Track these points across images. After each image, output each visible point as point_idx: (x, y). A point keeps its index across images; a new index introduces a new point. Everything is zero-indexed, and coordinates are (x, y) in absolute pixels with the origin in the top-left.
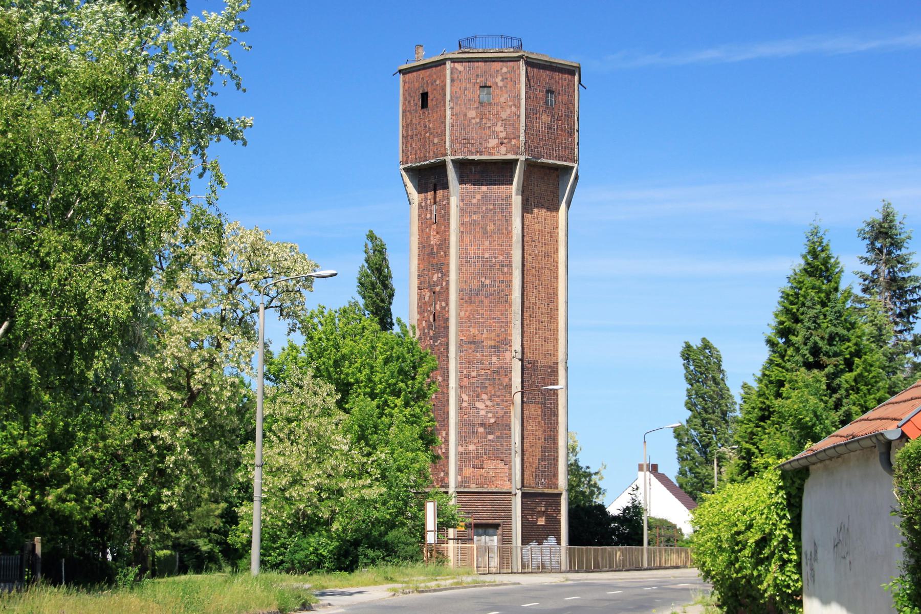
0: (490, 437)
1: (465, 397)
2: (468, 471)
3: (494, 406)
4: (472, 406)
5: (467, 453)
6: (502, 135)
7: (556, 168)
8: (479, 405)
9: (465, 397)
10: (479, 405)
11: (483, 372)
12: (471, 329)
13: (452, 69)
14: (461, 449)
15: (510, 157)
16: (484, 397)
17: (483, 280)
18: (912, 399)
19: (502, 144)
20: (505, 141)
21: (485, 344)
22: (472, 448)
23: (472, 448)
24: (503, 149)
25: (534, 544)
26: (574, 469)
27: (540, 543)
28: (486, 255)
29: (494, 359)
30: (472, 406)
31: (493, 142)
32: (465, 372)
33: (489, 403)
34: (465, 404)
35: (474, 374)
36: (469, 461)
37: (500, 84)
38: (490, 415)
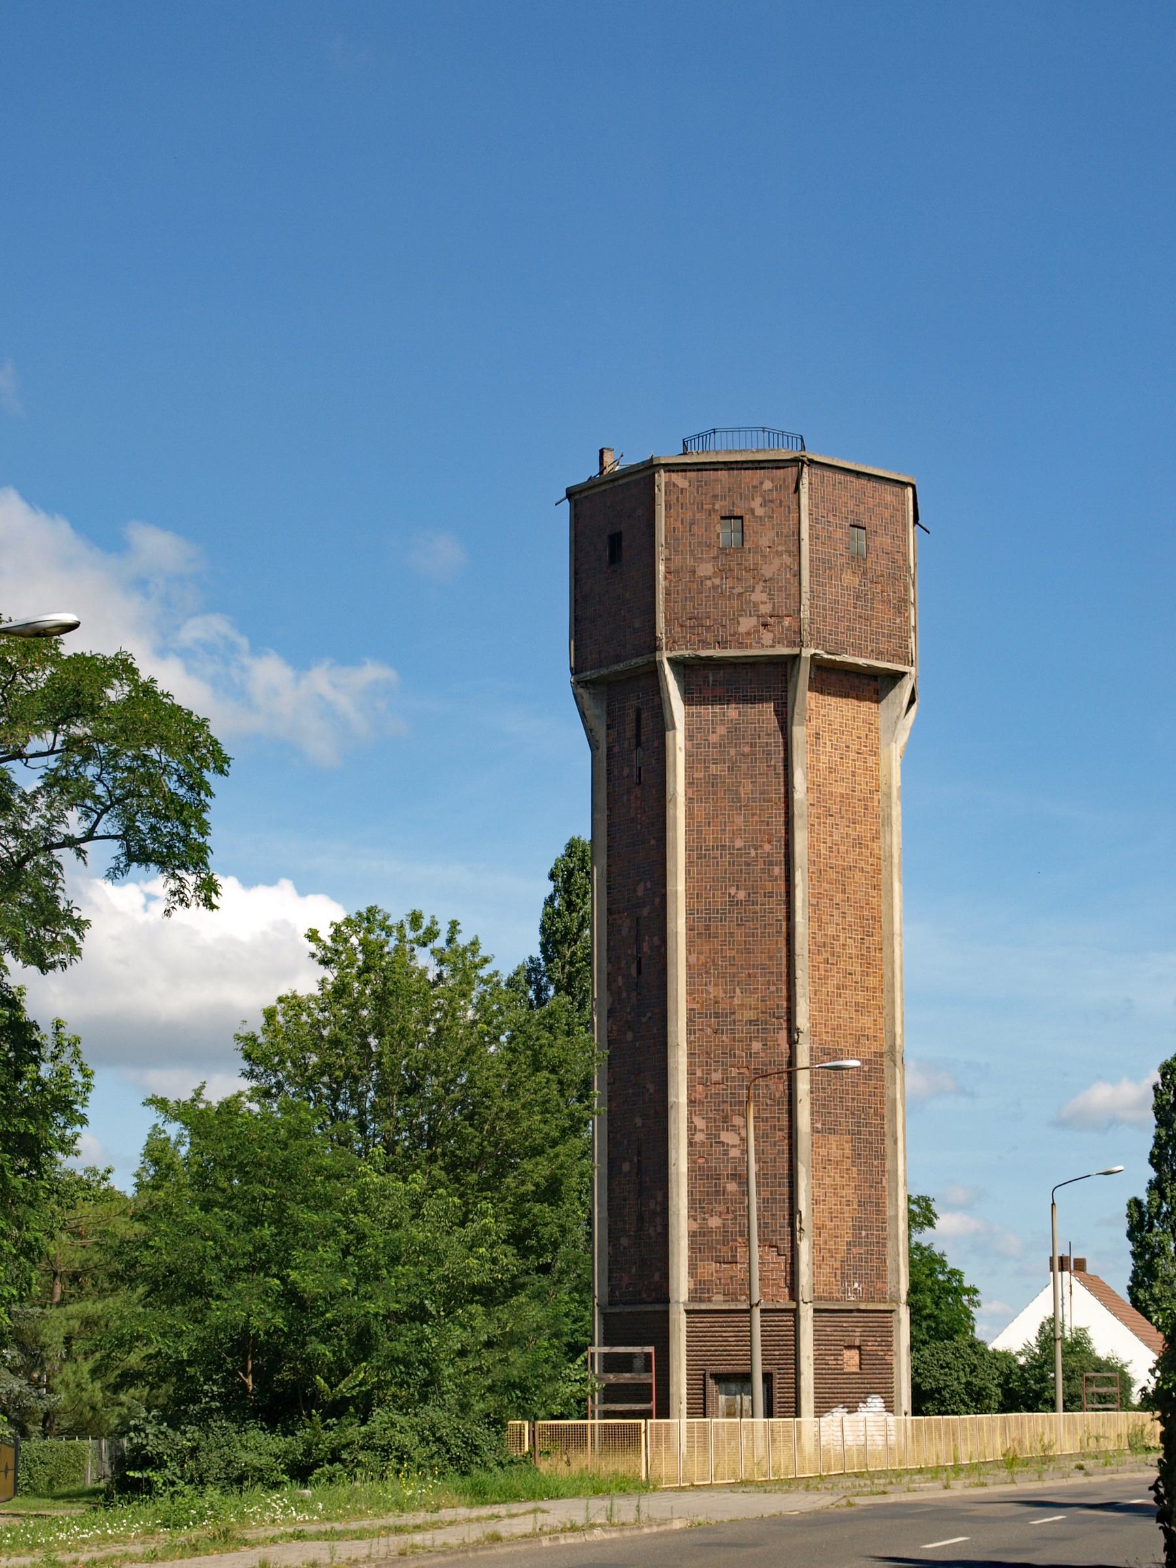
1: (700, 1123)
9: (700, 1123)
11: (734, 1072)
12: (711, 989)
17: (733, 891)
21: (738, 1017)
22: (714, 1222)
23: (714, 1222)
32: (699, 1074)
35: (716, 1076)
37: (759, 512)
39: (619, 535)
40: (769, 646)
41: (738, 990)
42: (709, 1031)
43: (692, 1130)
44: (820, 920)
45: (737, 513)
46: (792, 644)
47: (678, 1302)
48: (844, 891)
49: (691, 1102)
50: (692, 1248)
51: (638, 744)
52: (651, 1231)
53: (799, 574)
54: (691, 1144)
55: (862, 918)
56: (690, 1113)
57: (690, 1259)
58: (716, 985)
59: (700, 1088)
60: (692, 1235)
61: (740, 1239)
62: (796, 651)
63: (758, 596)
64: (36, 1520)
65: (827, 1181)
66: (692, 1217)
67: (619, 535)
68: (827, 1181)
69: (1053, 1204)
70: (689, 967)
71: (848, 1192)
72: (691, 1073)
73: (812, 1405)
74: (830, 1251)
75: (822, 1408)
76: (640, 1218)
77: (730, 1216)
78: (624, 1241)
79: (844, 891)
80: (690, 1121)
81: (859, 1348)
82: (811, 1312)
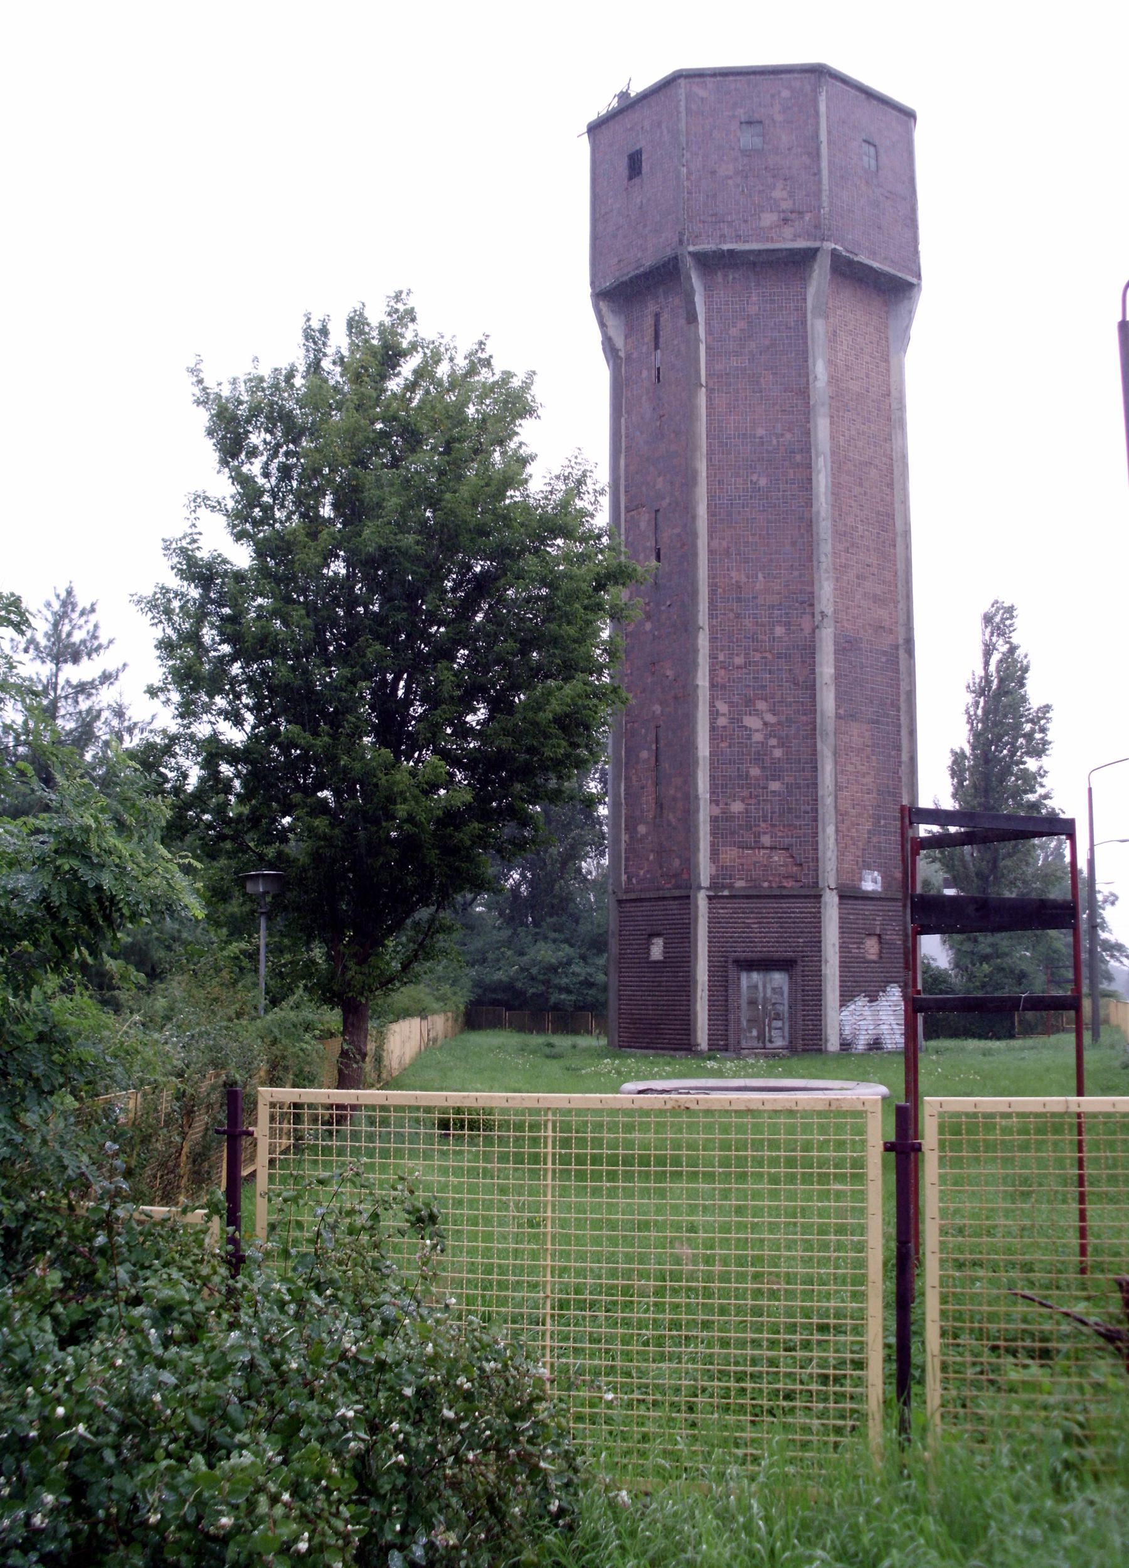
0: (775, 786)
1: (723, 707)
2: (729, 855)
3: (779, 723)
4: (736, 720)
5: (728, 817)
6: (786, 205)
7: (893, 279)
8: (752, 722)
9: (723, 707)
10: (752, 722)
11: (757, 657)
12: (734, 574)
13: (689, 97)
14: (717, 811)
15: (801, 244)
16: (761, 705)
17: (754, 478)
18: (1090, 790)
19: (786, 221)
20: (793, 216)
21: (760, 601)
22: (737, 807)
23: (737, 807)
24: (788, 232)
25: (861, 1001)
26: (1004, 715)
27: (873, 999)
28: (760, 432)
29: (779, 631)
30: (736, 720)
31: (769, 219)
32: (721, 658)
33: (770, 718)
34: (722, 721)
35: (739, 660)
36: (732, 833)
37: (779, 118)
38: (773, 742)
39: (639, 153)
40: (789, 240)
41: (760, 575)
42: (731, 615)
43: (714, 714)
44: (840, 509)
45: (757, 117)
46: (810, 236)
47: (699, 888)
48: (861, 485)
49: (713, 685)
50: (713, 834)
51: (656, 347)
52: (671, 816)
53: (818, 173)
54: (713, 729)
55: (878, 513)
56: (713, 699)
57: (712, 844)
58: (738, 570)
59: (722, 672)
60: (714, 820)
61: (763, 825)
62: (817, 244)
63: (778, 194)
64: (878, 1131)
65: (850, 768)
66: (714, 801)
67: (639, 153)
68: (850, 768)
69: (1090, 790)
70: (711, 552)
71: (868, 780)
72: (713, 657)
73: (837, 993)
74: (852, 838)
75: (846, 998)
76: (660, 806)
77: (753, 801)
78: (642, 829)
79: (861, 485)
80: (712, 705)
81: (879, 936)
82: (836, 899)
